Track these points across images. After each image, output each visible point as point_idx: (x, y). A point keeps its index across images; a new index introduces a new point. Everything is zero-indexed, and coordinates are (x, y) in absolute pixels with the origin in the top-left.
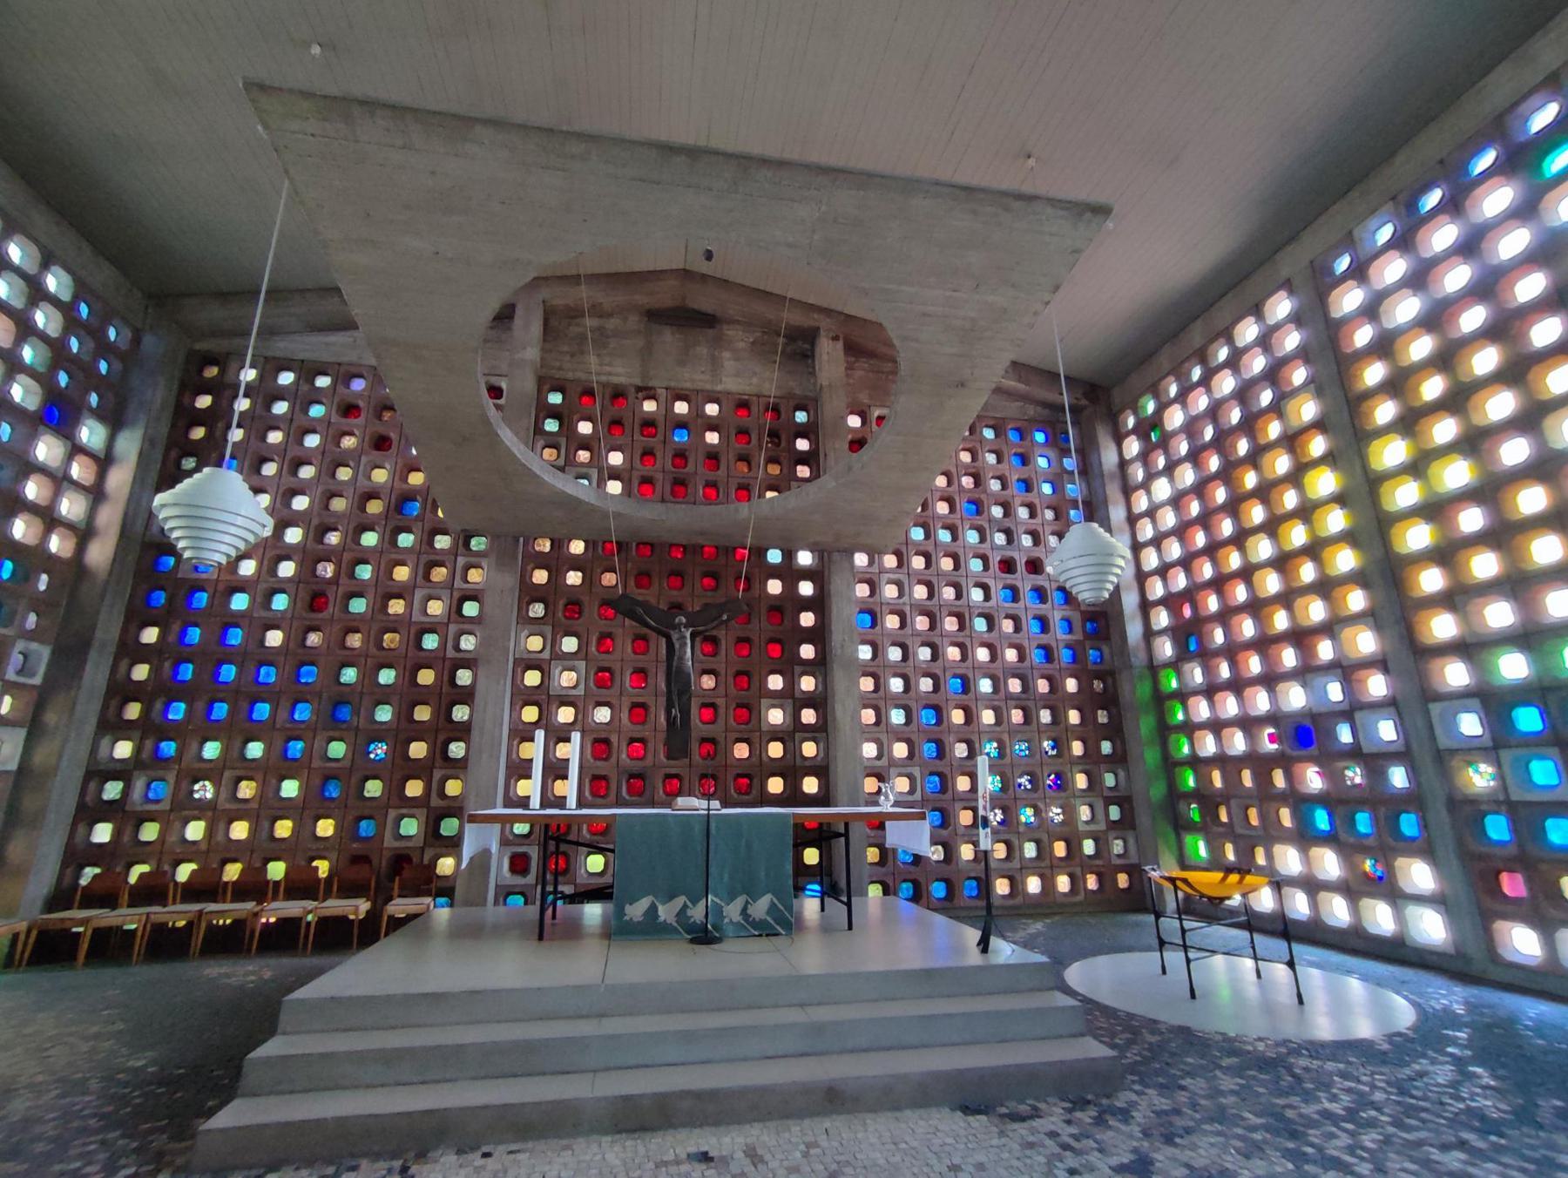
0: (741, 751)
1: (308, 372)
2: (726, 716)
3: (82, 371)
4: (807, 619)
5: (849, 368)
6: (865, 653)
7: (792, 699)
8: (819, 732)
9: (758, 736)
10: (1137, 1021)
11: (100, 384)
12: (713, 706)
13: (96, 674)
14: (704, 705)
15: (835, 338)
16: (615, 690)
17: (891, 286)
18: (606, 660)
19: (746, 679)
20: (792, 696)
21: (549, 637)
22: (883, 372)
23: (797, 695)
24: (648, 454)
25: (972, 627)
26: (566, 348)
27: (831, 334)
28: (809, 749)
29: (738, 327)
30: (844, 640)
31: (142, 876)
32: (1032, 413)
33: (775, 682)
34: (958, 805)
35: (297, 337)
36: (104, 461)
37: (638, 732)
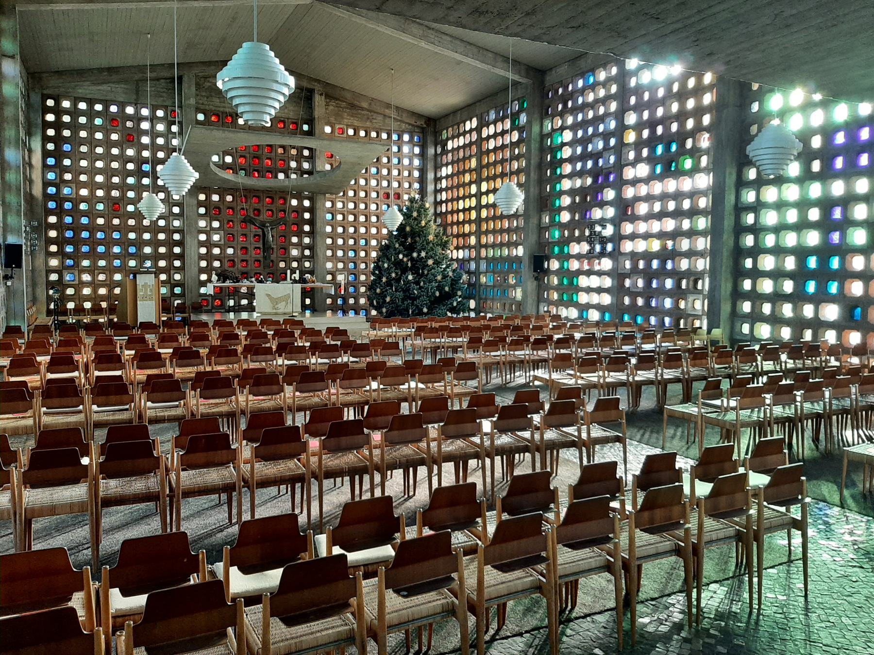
1: (91, 103)
4: (307, 216)
5: (327, 105)
6: (329, 229)
7: (300, 245)
8: (311, 258)
9: (288, 260)
14: (229, 260)
15: (321, 95)
16: (235, 242)
18: (231, 231)
19: (286, 237)
20: (301, 245)
21: (58, 174)
23: (303, 245)
25: (370, 220)
26: (204, 94)
27: (320, 93)
28: (307, 264)
31: (178, 304)
32: (404, 127)
33: (295, 240)
34: (360, 285)
37: (245, 257)
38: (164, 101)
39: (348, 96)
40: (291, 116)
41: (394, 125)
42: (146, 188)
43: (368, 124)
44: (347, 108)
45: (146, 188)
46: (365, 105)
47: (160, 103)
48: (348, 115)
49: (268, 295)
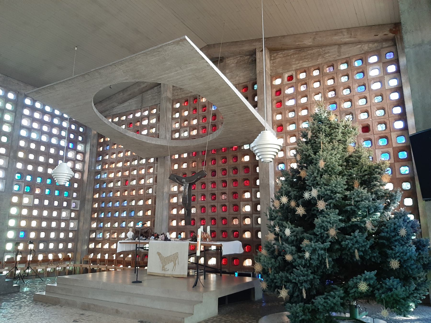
0: (236, 222)
2: (231, 210)
3: (77, 133)
10: (17, 299)
11: (81, 134)
12: (225, 205)
13: (88, 207)
17: (160, 77)
22: (289, 56)
24: (204, 118)
29: (231, 58)
30: (264, 177)
31: (8, 259)
35: (118, 107)
36: (84, 153)
38: (155, 102)
39: (288, 41)
40: (241, 82)
41: (355, 50)
42: (61, 158)
43: (320, 61)
44: (296, 54)
45: (61, 158)
46: (308, 42)
47: (153, 104)
48: (296, 60)
49: (159, 254)
